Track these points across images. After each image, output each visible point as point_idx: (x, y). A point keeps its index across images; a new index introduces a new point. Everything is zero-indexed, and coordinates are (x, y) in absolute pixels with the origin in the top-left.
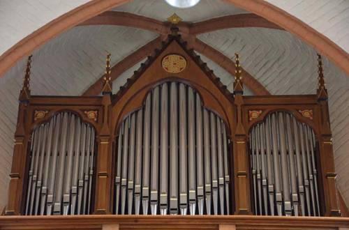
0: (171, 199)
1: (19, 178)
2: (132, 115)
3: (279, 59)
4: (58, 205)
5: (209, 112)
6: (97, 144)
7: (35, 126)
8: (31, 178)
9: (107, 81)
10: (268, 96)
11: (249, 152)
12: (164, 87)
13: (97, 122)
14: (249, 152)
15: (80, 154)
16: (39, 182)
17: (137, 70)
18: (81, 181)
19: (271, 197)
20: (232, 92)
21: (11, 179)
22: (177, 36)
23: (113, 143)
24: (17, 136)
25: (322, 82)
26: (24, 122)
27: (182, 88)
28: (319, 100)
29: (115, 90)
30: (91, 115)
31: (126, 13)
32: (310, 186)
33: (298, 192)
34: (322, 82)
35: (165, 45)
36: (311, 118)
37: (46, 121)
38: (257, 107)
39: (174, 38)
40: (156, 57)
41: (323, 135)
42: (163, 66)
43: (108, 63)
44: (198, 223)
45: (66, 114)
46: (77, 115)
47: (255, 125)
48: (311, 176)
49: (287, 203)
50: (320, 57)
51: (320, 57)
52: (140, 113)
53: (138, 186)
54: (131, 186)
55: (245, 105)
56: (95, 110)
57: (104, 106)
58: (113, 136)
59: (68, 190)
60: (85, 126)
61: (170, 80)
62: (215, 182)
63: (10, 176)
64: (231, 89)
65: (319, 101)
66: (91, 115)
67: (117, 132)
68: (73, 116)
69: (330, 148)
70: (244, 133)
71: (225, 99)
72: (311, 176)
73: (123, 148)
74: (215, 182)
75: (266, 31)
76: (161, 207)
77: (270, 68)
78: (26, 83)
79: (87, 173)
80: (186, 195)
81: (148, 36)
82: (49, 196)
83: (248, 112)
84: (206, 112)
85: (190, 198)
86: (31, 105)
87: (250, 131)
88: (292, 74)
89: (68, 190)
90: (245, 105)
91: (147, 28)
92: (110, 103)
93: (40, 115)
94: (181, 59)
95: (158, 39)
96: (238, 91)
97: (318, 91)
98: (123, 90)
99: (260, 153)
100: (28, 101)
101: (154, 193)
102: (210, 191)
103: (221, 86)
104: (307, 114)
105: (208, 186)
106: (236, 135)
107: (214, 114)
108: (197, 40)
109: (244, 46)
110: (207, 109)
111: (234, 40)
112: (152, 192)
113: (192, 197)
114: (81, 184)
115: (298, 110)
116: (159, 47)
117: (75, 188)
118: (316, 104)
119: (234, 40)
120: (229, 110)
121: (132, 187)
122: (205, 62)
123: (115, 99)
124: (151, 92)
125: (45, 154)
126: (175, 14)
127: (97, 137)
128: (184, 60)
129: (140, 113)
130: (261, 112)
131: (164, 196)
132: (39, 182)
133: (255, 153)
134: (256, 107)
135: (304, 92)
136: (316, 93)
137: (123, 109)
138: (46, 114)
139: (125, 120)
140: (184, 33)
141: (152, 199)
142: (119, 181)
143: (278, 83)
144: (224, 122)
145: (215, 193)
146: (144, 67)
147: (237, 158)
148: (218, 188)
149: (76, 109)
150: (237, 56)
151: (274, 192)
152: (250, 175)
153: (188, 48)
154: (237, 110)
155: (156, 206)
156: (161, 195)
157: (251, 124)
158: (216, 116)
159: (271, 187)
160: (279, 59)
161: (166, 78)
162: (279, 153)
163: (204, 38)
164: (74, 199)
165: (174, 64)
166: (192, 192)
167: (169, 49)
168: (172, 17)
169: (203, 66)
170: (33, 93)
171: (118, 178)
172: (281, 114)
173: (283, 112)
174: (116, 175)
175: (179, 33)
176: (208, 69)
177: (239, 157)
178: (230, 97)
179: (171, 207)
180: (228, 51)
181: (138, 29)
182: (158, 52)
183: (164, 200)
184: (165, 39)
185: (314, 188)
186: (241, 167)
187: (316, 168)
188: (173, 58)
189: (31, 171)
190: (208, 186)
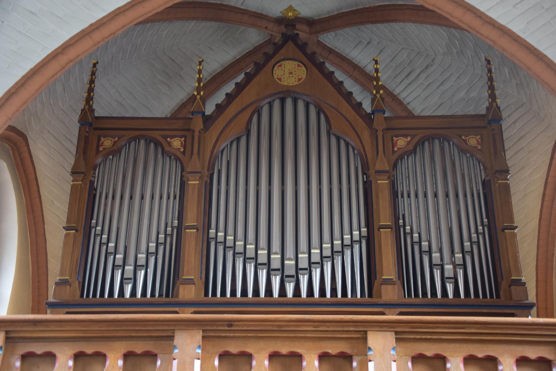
0: (286, 262)
1: (77, 231)
2: (231, 143)
3: (427, 67)
4: (129, 268)
5: (338, 139)
6: (183, 185)
7: (99, 160)
8: (93, 230)
9: (198, 97)
10: (411, 115)
11: (395, 195)
12: (277, 105)
13: (184, 153)
14: (395, 195)
15: (161, 198)
16: (105, 236)
17: (219, 102)
18: (162, 236)
19: (426, 259)
20: (369, 110)
21: (65, 232)
22: (292, 35)
23: (206, 182)
24: (74, 172)
25: (493, 96)
26: (85, 153)
27: (301, 106)
28: (490, 122)
29: (209, 109)
30: (177, 143)
31: (226, 6)
32: (478, 242)
33: (463, 252)
34: (493, 96)
35: (278, 48)
36: (479, 147)
37: (115, 152)
38: (404, 132)
39: (290, 38)
40: (265, 64)
41: (497, 171)
42: (275, 76)
43: (200, 72)
44: (331, 329)
45: (142, 142)
46: (157, 144)
47: (401, 158)
48: (480, 228)
49: (448, 267)
50: (489, 62)
51: (489, 62)
52: (243, 141)
53: (240, 243)
54: (230, 243)
55: (388, 129)
56: (181, 137)
57: (194, 132)
58: (206, 173)
59: (143, 247)
60: (168, 159)
61: (284, 95)
62: (347, 237)
63: (64, 228)
64: (367, 107)
65: (489, 123)
66: (177, 143)
67: (211, 167)
68: (152, 145)
69: (507, 188)
70: (388, 169)
71: (360, 120)
72: (480, 228)
73: (220, 188)
74: (347, 237)
75: (412, 29)
76: (272, 272)
77: (414, 80)
78: (89, 99)
79: (169, 224)
80: (307, 255)
81: (253, 37)
82: (117, 256)
83: (393, 140)
84: (334, 140)
85: (313, 260)
86: (95, 129)
87: (395, 166)
88: (443, 88)
89: (143, 247)
90: (388, 129)
91: (253, 25)
92: (202, 127)
93: (107, 143)
94: (299, 66)
95: (268, 42)
96: (377, 110)
97: (488, 108)
98: (220, 108)
99: (409, 196)
100: (91, 125)
101: (263, 253)
102: (340, 250)
103: (354, 102)
104: (473, 141)
105: (337, 242)
106: (377, 172)
107: (345, 141)
108: (319, 43)
109: (381, 51)
110: (335, 135)
111: (369, 43)
112: (259, 252)
113: (316, 258)
114: (161, 240)
115: (460, 136)
116: (270, 50)
117: (153, 245)
118: (485, 127)
119: (369, 43)
120: (366, 136)
121: (232, 245)
122: (340, 79)
123: (208, 120)
124: (258, 111)
125: (113, 198)
126: (291, 6)
127: (183, 173)
128: (304, 68)
129: (243, 141)
130: (409, 138)
131: (276, 257)
132: (105, 236)
133: (402, 196)
134: (403, 132)
135: (471, 110)
136: (484, 113)
137: (220, 135)
138: (115, 142)
139: (222, 151)
140: (303, 33)
141: (259, 261)
142: (214, 236)
143: (422, 99)
144: (360, 153)
145: (348, 253)
146: (240, 87)
147: (377, 197)
148: (352, 246)
149: (157, 135)
150: (376, 62)
151: (430, 252)
152: (397, 229)
153: (309, 52)
154: (377, 136)
155: (265, 271)
156: (272, 256)
157: (396, 156)
158: (347, 144)
159: (425, 244)
160: (427, 67)
161: (279, 93)
162: (436, 195)
163: (330, 39)
164: (161, 248)
165: (289, 72)
166: (315, 251)
167: (283, 52)
168: (286, 10)
169: (330, 76)
170: (96, 115)
171: (212, 231)
172: (437, 142)
173: (439, 139)
174: (209, 227)
175: (296, 32)
176: (337, 79)
177: (381, 201)
178: (368, 118)
179: (286, 273)
180: (363, 58)
181: (243, 28)
182: (268, 57)
183: (276, 263)
184: (278, 39)
185: (484, 243)
186: (384, 217)
187: (488, 217)
188: (289, 65)
189: (94, 221)
190: (337, 242)
